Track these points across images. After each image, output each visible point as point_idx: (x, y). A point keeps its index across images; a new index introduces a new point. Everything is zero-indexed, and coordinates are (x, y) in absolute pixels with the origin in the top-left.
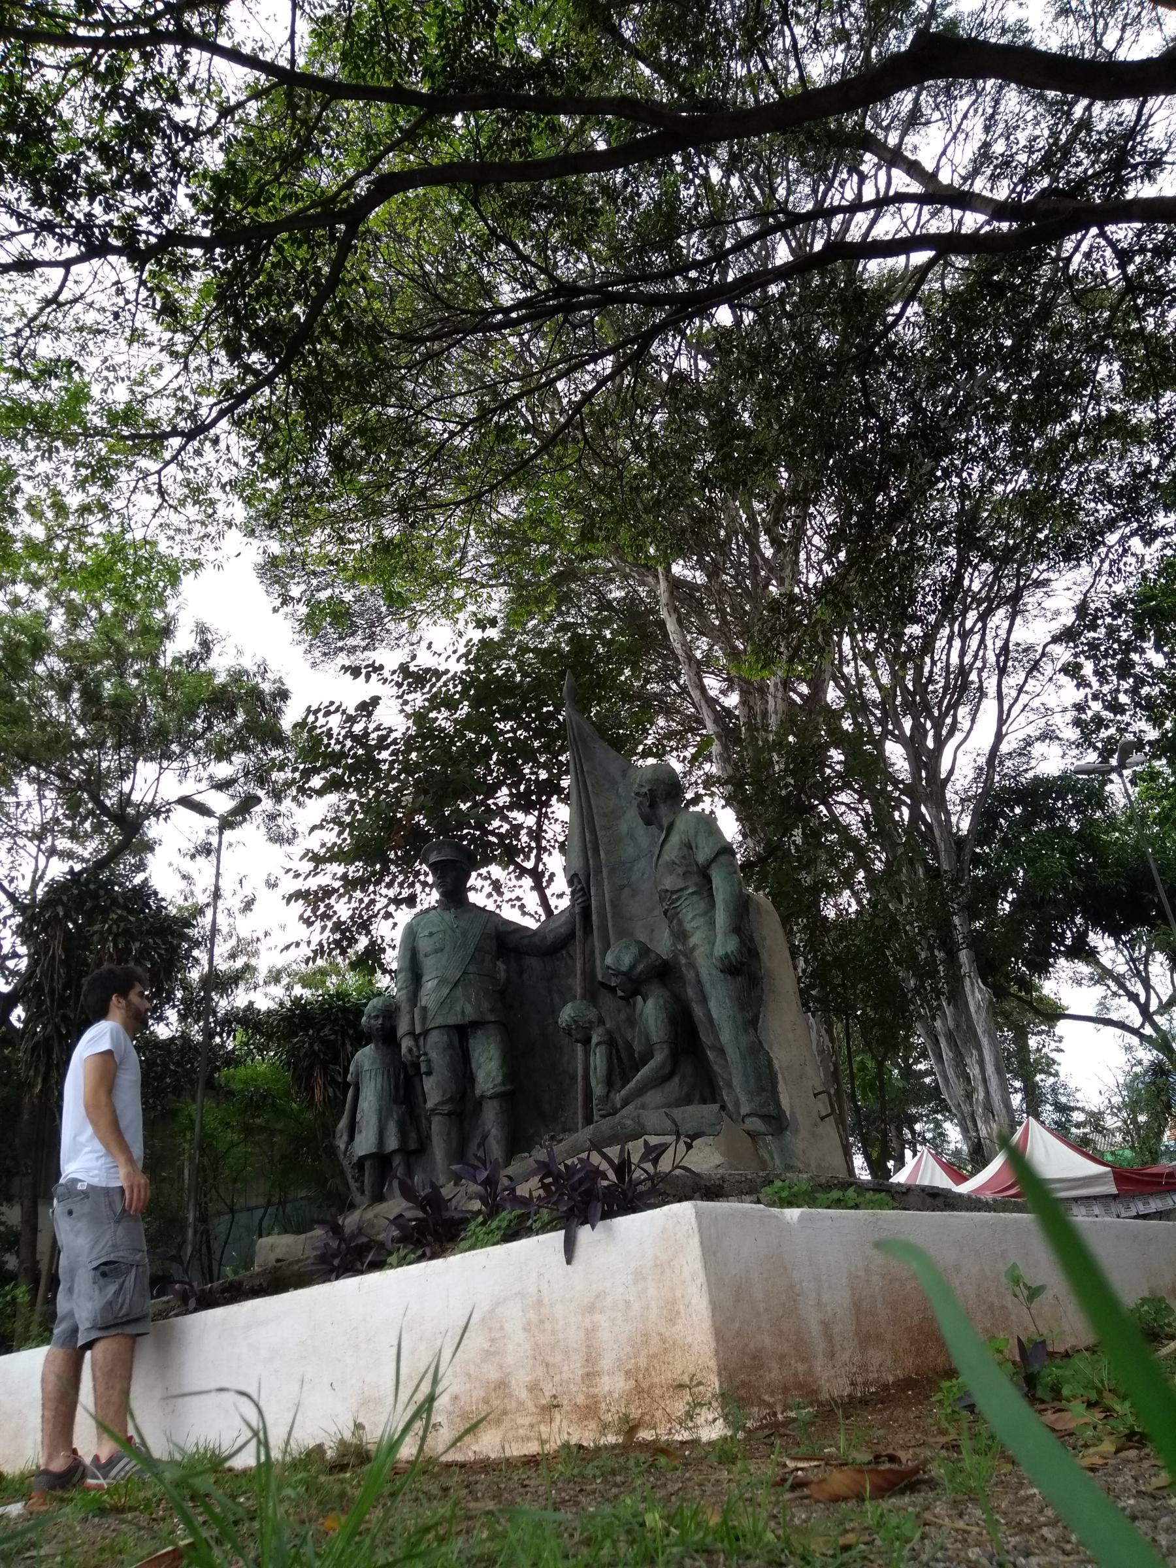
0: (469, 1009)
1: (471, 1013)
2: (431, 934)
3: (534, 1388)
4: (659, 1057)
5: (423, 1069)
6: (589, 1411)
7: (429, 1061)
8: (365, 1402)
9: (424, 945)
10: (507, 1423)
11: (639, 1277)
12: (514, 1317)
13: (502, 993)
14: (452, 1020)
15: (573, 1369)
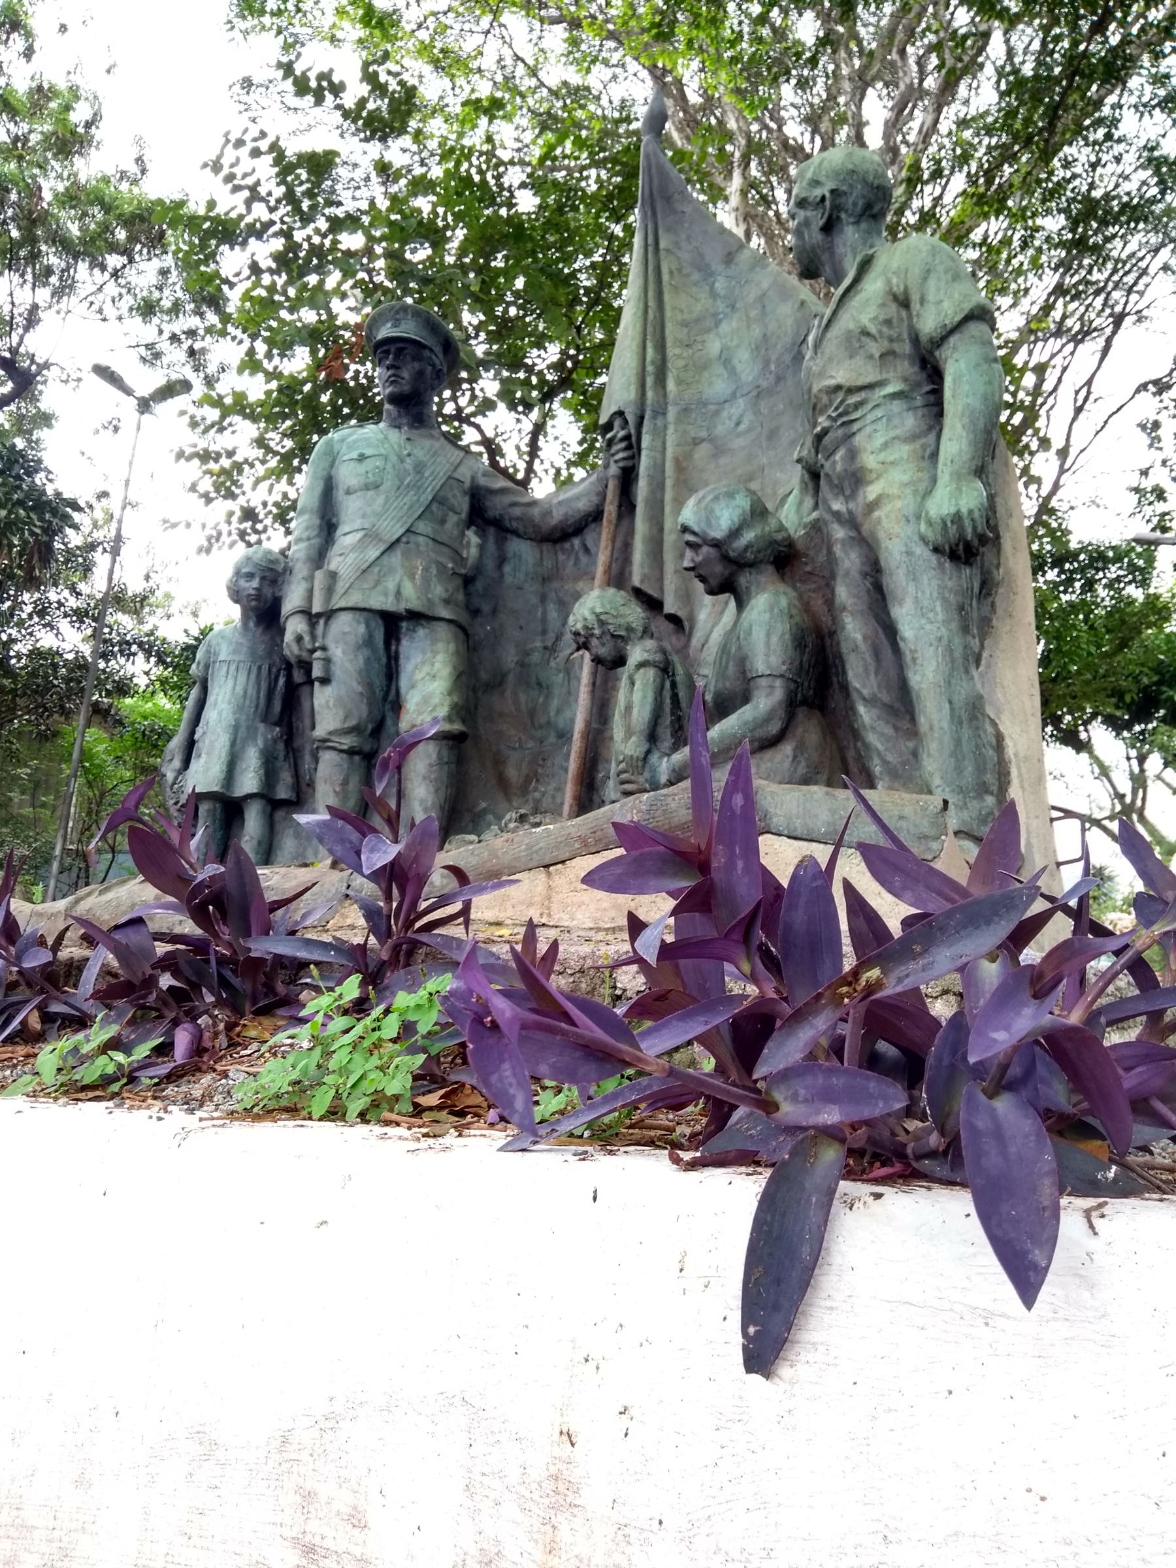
1: (412, 598)
2: (362, 458)
4: (765, 702)
5: (317, 672)
7: (328, 661)
13: (468, 581)
14: (378, 601)
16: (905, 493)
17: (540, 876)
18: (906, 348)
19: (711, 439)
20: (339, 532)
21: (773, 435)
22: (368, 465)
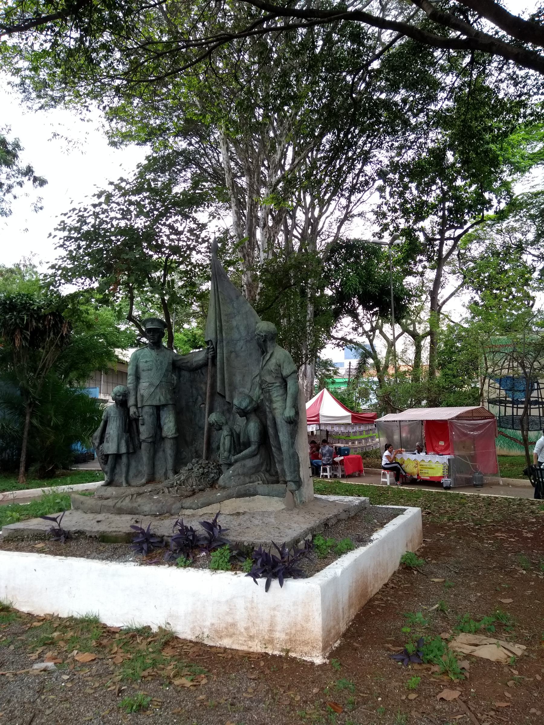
0: (162, 399)
1: (163, 402)
2: (146, 362)
3: (247, 629)
4: (253, 448)
6: (271, 641)
7: (143, 419)
8: (171, 616)
9: (142, 365)
10: (235, 637)
11: (295, 604)
12: (241, 604)
14: (155, 403)
15: (265, 627)
16: (281, 410)
17: (219, 504)
18: (280, 375)
19: (235, 352)
20: (141, 381)
21: (251, 354)
22: (148, 364)
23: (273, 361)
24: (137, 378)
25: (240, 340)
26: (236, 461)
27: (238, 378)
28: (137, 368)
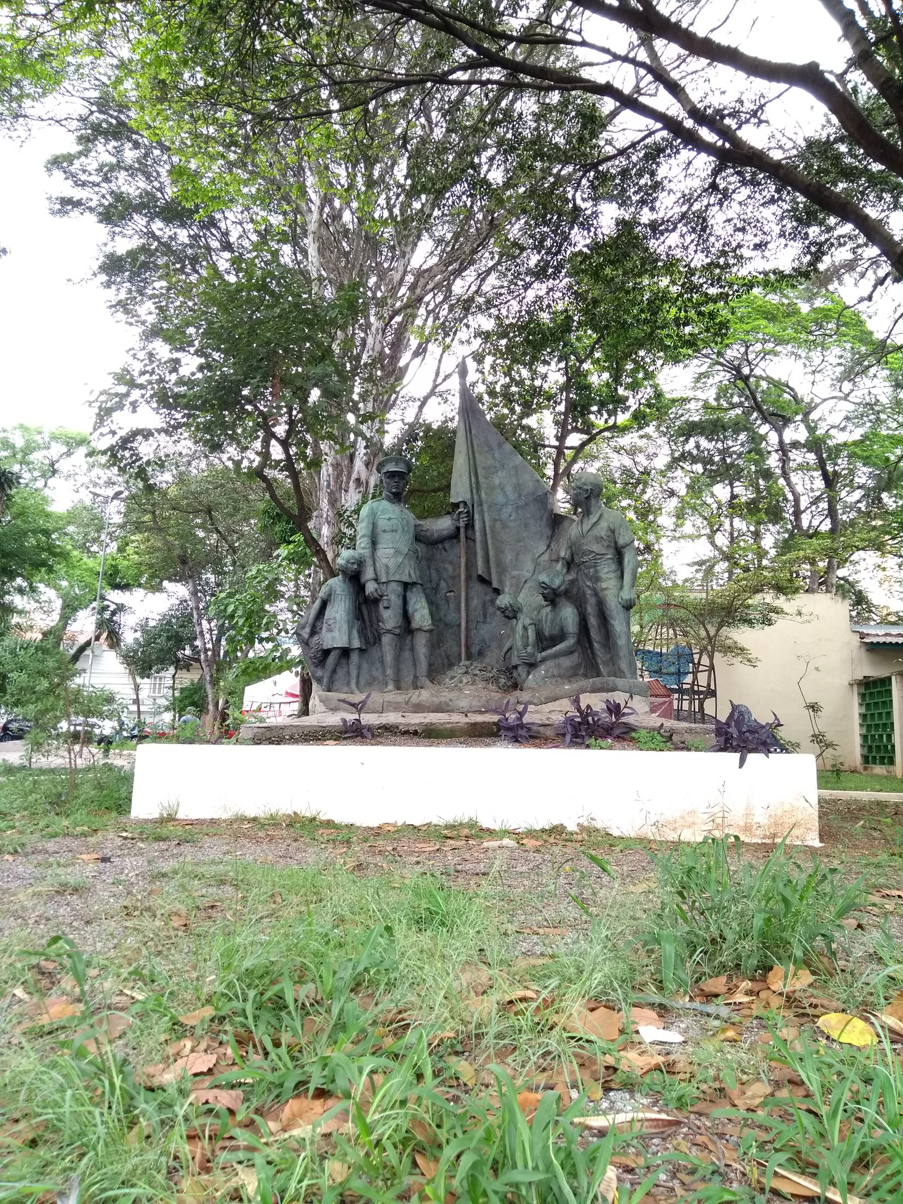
4: (570, 642)
9: (382, 524)
14: (405, 579)
20: (380, 546)
23: (604, 524)
24: (374, 543)
25: (506, 504)
26: (543, 660)
27: (508, 557)
28: (374, 526)
